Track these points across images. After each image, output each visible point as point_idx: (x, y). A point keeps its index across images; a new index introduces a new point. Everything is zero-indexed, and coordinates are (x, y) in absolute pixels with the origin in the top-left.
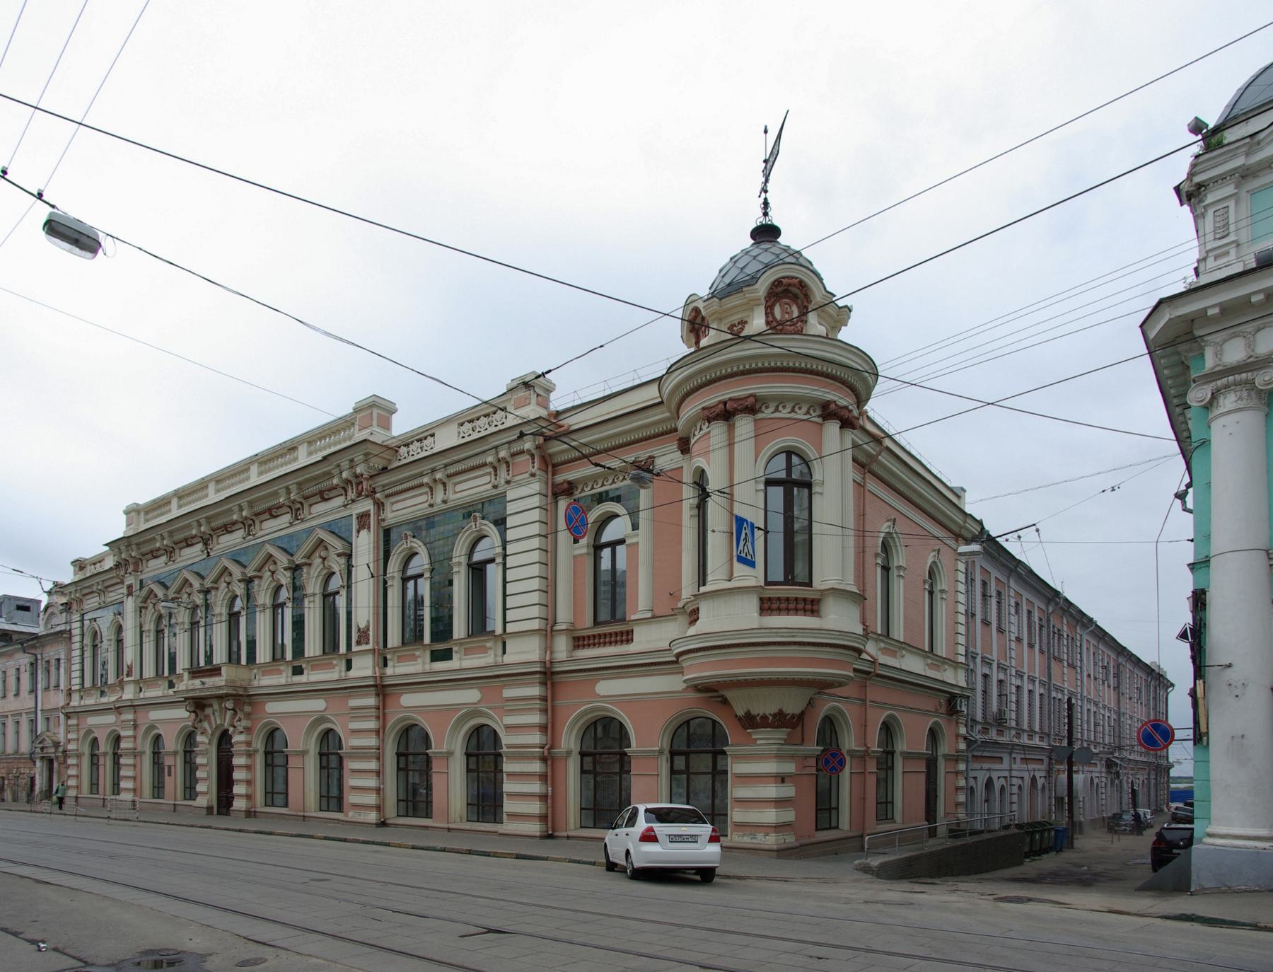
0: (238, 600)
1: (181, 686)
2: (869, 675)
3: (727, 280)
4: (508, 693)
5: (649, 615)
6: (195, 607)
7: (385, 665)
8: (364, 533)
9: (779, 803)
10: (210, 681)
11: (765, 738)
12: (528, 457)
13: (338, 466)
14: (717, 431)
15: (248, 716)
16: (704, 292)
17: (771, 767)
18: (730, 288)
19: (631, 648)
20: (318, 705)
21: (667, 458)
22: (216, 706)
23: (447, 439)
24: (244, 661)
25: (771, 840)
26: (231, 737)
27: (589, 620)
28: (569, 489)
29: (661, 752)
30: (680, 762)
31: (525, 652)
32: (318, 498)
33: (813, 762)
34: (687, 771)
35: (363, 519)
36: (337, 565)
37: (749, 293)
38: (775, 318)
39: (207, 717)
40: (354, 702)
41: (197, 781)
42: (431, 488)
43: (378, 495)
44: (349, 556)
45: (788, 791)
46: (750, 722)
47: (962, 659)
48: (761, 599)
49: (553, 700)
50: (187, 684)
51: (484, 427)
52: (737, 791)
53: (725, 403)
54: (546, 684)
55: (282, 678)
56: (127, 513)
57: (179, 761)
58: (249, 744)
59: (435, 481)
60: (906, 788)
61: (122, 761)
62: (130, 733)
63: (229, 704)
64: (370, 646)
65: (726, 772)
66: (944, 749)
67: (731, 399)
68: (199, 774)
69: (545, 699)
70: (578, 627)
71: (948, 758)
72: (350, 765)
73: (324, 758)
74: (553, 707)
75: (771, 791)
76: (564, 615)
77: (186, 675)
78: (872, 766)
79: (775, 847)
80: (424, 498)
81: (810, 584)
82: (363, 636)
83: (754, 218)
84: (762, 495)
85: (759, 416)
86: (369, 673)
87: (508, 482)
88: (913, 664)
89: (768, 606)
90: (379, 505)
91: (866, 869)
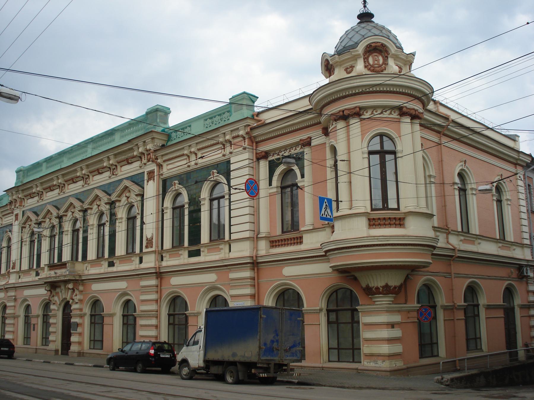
0: (78, 222)
1: (43, 275)
2: (451, 257)
3: (343, 44)
4: (232, 275)
5: (311, 228)
6: (53, 227)
7: (162, 260)
8: (151, 182)
9: (390, 341)
10: (60, 272)
11: (384, 301)
12: (242, 139)
13: (137, 145)
14: (341, 124)
15: (81, 292)
16: (332, 51)
17: (383, 318)
18: (344, 49)
19: (302, 247)
20: (122, 285)
21: (318, 139)
22: (63, 287)
23: (197, 129)
24: (80, 259)
25: (385, 365)
26: (71, 306)
27: (279, 231)
28: (265, 155)
29: (321, 310)
30: (333, 317)
31: (242, 251)
32: (125, 162)
33: (415, 314)
34: (337, 322)
35: (151, 174)
36: (134, 199)
37: (354, 52)
38: (369, 64)
39: (57, 294)
40: (144, 283)
41: (50, 333)
42: (189, 156)
43: (159, 161)
44: (142, 196)
45: (397, 333)
46: (370, 292)
47: (527, 242)
48: (369, 219)
49: (258, 279)
50: (46, 274)
51: (218, 122)
52: (365, 334)
53: (343, 111)
54: (254, 270)
55: (103, 268)
56: (17, 172)
57: (40, 321)
58: (81, 310)
59: (191, 152)
60: (489, 330)
61: (7, 321)
62: (12, 304)
63: (70, 286)
64: (153, 249)
65: (358, 322)
66: (518, 301)
67: (346, 109)
68: (51, 329)
69: (253, 279)
70: (272, 235)
71: (522, 307)
72: (141, 322)
73: (125, 318)
74: (258, 283)
75: (385, 333)
76: (264, 228)
77: (46, 268)
78: (460, 315)
79: (388, 369)
80: (185, 162)
81: (398, 209)
82: (150, 242)
83: (359, 9)
84: (366, 161)
85: (363, 117)
86: (152, 265)
87: (231, 153)
88: (489, 248)
89: (373, 223)
90: (160, 166)
91: (440, 382)
